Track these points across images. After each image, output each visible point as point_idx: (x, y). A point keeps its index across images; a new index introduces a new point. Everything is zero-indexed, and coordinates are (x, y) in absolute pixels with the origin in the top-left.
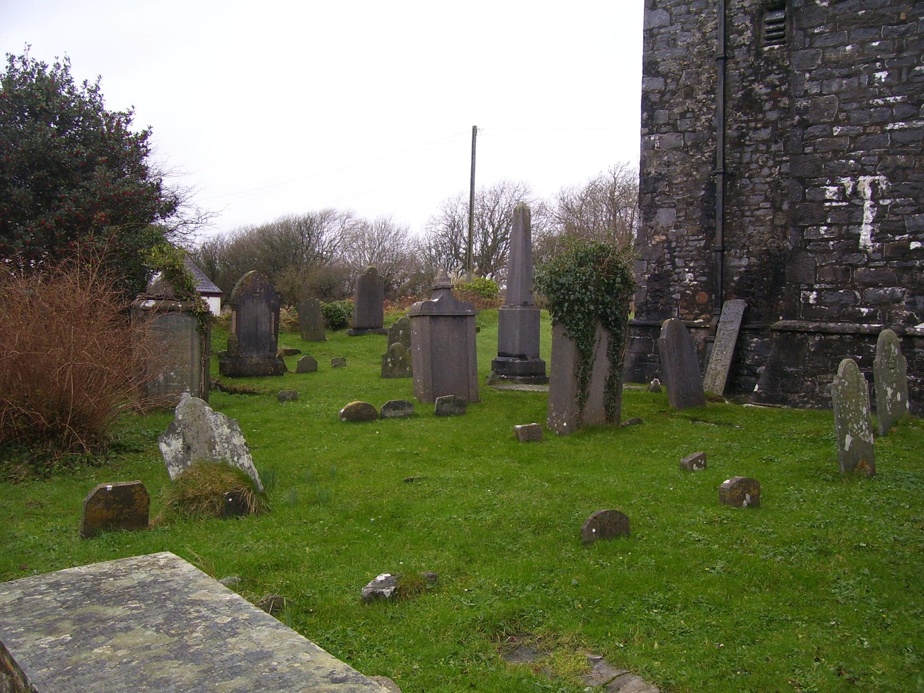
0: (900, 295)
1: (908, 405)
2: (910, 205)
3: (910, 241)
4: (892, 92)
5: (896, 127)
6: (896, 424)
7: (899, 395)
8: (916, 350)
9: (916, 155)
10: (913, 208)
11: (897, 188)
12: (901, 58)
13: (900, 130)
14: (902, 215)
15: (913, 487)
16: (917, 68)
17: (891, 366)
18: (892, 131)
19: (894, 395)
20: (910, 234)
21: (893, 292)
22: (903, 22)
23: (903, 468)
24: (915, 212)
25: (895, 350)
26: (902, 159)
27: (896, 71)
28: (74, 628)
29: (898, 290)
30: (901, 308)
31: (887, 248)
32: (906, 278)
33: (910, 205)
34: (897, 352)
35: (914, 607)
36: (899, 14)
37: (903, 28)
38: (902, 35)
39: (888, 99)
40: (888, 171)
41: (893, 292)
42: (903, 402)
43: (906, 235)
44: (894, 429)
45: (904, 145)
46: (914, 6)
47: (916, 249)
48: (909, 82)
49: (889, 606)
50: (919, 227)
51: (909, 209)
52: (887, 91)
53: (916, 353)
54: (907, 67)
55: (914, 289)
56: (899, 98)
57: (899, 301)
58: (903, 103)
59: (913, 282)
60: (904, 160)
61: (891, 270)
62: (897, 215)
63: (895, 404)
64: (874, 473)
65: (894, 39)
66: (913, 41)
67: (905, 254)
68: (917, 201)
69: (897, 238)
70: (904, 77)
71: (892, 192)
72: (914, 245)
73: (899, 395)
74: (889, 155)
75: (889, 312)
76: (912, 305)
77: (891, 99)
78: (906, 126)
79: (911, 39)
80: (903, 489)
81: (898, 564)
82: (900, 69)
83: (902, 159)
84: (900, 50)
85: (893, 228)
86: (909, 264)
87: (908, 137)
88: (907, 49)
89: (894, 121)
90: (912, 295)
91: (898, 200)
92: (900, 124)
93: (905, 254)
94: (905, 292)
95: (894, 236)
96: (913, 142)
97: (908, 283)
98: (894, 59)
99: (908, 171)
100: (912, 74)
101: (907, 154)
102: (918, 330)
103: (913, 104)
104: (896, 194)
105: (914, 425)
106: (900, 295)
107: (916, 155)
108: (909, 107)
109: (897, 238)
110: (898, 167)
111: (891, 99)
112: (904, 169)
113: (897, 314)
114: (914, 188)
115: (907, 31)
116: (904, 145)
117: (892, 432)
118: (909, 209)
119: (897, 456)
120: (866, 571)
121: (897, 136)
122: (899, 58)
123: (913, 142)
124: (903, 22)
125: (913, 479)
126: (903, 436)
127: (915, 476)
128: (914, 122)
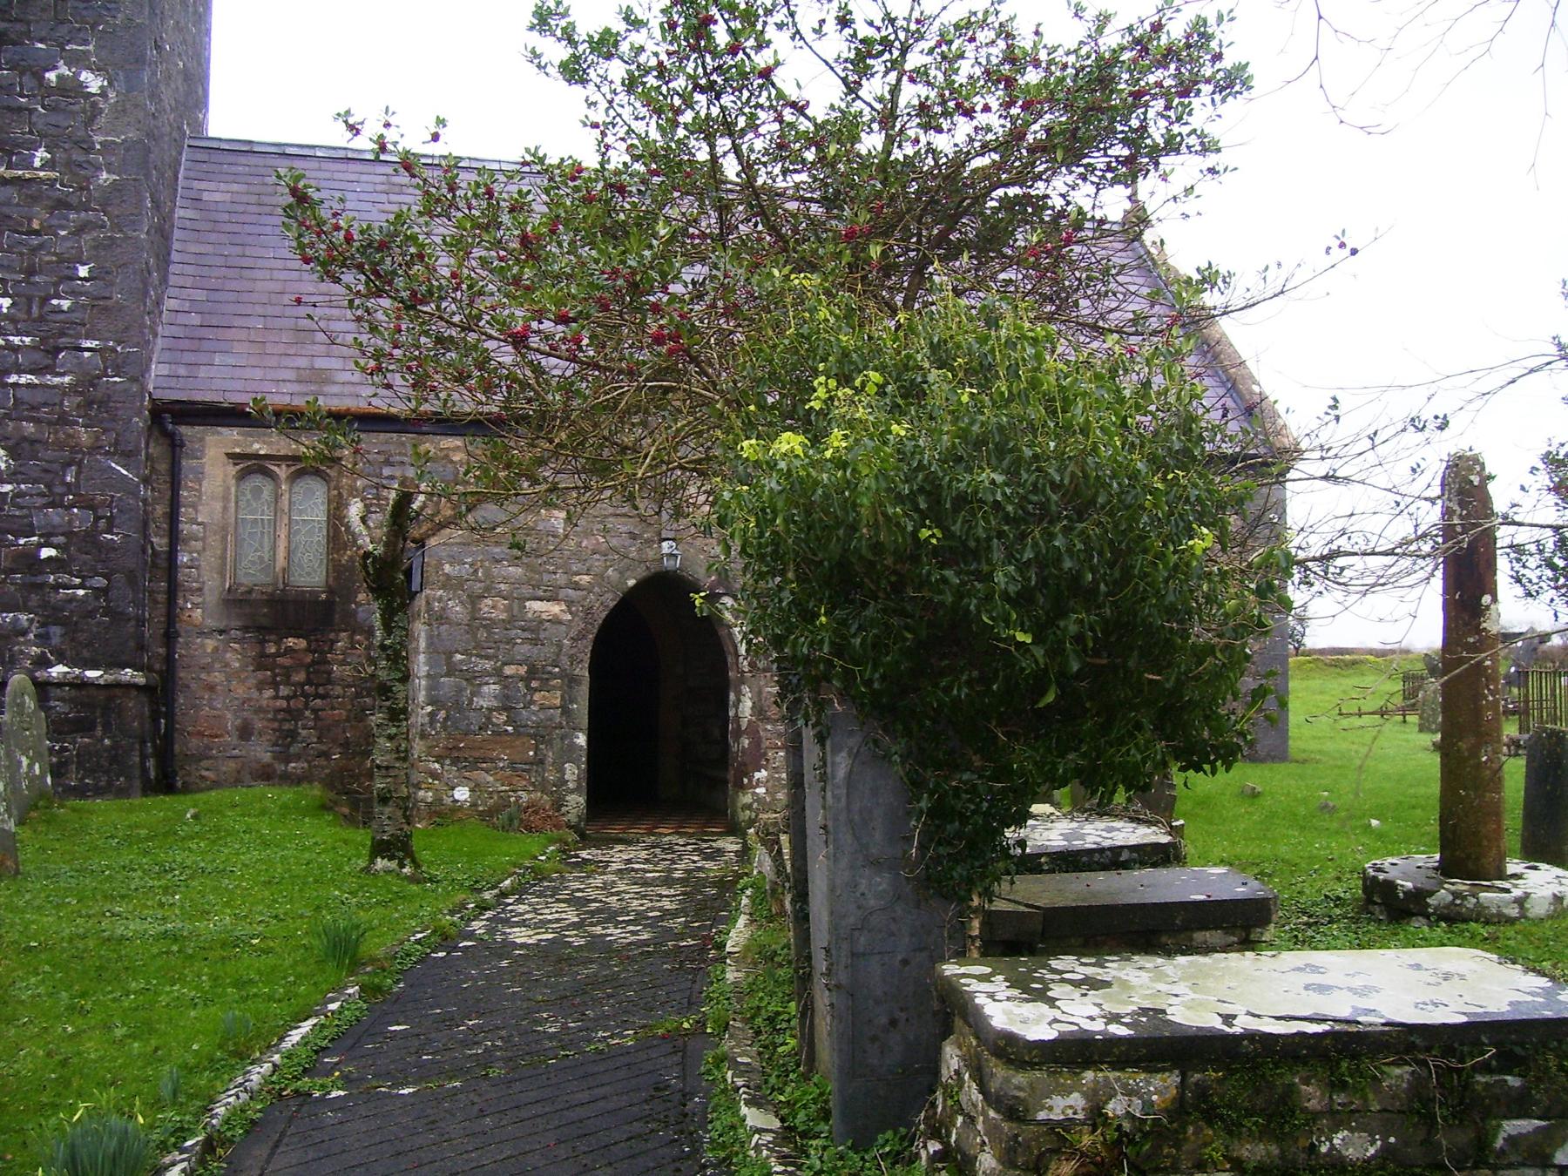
0: (26, 624)
1: (49, 780)
2: (42, 495)
3: (40, 546)
4: (17, 329)
5: (23, 381)
6: (36, 807)
7: (37, 766)
8: (52, 704)
9: (50, 423)
10: (45, 500)
11: (22, 469)
12: (33, 284)
13: (29, 385)
14: (29, 508)
15: (73, 880)
16: (55, 302)
17: (25, 726)
18: (16, 385)
19: (31, 766)
20: (40, 536)
21: (15, 620)
22: (37, 233)
23: (55, 863)
24: (47, 506)
25: (30, 703)
26: (29, 428)
27: (24, 299)
28: (767, 488)
29: (23, 617)
30: (28, 643)
31: (6, 556)
32: (34, 599)
33: (42, 495)
34: (32, 706)
35: (111, 992)
36: (30, 220)
37: (35, 241)
38: (34, 250)
39: (11, 338)
40: (11, 443)
41: (15, 620)
42: (42, 776)
43: (35, 538)
44: (34, 814)
45: (33, 408)
46: (51, 214)
47: (50, 558)
48: (42, 319)
49: (83, 995)
50: (54, 527)
51: (40, 501)
52: (11, 327)
53: (52, 708)
54: (40, 297)
55: (48, 617)
56: (27, 340)
57: (24, 633)
58: (33, 348)
59: (45, 605)
60: (33, 430)
61: (13, 588)
62: (22, 508)
63: (32, 779)
64: (17, 872)
65: (22, 254)
66: (49, 263)
67: (33, 564)
68: (50, 490)
69: (22, 541)
70: (35, 310)
71: (15, 473)
72: (46, 553)
73: (37, 766)
74: (11, 420)
75: (10, 650)
76: (43, 639)
77: (16, 340)
78: (36, 381)
79: (47, 258)
80: (62, 884)
81: (82, 958)
82: (30, 300)
83: (29, 428)
84: (31, 272)
85: (15, 527)
86: (39, 579)
87: (39, 397)
88: (40, 273)
89: (19, 372)
90: (43, 625)
91: (23, 486)
92: (29, 376)
93: (33, 564)
94: (32, 619)
95: (17, 537)
96: (45, 404)
97: (39, 606)
98: (21, 282)
99: (38, 446)
100: (46, 309)
101: (37, 421)
102: (54, 675)
103: (47, 352)
104: (20, 477)
105: (61, 806)
106: (26, 624)
107: (50, 423)
108: (42, 354)
109: (22, 541)
110: (25, 439)
111: (16, 340)
112: (33, 442)
113: (22, 652)
114: (46, 471)
115: (41, 246)
116: (33, 408)
117: (30, 819)
118: (40, 501)
119: (43, 849)
120: (47, 968)
121: (24, 394)
122: (28, 283)
123: (45, 404)
124: (37, 233)
125: (73, 873)
126: (48, 822)
127: (72, 870)
128: (49, 377)
